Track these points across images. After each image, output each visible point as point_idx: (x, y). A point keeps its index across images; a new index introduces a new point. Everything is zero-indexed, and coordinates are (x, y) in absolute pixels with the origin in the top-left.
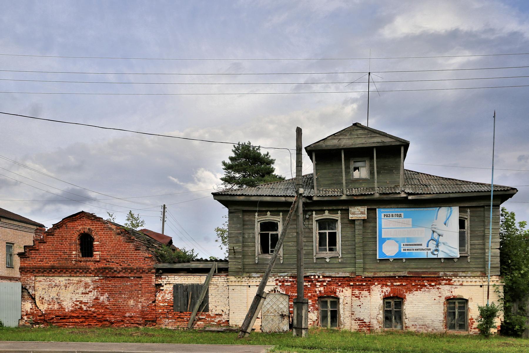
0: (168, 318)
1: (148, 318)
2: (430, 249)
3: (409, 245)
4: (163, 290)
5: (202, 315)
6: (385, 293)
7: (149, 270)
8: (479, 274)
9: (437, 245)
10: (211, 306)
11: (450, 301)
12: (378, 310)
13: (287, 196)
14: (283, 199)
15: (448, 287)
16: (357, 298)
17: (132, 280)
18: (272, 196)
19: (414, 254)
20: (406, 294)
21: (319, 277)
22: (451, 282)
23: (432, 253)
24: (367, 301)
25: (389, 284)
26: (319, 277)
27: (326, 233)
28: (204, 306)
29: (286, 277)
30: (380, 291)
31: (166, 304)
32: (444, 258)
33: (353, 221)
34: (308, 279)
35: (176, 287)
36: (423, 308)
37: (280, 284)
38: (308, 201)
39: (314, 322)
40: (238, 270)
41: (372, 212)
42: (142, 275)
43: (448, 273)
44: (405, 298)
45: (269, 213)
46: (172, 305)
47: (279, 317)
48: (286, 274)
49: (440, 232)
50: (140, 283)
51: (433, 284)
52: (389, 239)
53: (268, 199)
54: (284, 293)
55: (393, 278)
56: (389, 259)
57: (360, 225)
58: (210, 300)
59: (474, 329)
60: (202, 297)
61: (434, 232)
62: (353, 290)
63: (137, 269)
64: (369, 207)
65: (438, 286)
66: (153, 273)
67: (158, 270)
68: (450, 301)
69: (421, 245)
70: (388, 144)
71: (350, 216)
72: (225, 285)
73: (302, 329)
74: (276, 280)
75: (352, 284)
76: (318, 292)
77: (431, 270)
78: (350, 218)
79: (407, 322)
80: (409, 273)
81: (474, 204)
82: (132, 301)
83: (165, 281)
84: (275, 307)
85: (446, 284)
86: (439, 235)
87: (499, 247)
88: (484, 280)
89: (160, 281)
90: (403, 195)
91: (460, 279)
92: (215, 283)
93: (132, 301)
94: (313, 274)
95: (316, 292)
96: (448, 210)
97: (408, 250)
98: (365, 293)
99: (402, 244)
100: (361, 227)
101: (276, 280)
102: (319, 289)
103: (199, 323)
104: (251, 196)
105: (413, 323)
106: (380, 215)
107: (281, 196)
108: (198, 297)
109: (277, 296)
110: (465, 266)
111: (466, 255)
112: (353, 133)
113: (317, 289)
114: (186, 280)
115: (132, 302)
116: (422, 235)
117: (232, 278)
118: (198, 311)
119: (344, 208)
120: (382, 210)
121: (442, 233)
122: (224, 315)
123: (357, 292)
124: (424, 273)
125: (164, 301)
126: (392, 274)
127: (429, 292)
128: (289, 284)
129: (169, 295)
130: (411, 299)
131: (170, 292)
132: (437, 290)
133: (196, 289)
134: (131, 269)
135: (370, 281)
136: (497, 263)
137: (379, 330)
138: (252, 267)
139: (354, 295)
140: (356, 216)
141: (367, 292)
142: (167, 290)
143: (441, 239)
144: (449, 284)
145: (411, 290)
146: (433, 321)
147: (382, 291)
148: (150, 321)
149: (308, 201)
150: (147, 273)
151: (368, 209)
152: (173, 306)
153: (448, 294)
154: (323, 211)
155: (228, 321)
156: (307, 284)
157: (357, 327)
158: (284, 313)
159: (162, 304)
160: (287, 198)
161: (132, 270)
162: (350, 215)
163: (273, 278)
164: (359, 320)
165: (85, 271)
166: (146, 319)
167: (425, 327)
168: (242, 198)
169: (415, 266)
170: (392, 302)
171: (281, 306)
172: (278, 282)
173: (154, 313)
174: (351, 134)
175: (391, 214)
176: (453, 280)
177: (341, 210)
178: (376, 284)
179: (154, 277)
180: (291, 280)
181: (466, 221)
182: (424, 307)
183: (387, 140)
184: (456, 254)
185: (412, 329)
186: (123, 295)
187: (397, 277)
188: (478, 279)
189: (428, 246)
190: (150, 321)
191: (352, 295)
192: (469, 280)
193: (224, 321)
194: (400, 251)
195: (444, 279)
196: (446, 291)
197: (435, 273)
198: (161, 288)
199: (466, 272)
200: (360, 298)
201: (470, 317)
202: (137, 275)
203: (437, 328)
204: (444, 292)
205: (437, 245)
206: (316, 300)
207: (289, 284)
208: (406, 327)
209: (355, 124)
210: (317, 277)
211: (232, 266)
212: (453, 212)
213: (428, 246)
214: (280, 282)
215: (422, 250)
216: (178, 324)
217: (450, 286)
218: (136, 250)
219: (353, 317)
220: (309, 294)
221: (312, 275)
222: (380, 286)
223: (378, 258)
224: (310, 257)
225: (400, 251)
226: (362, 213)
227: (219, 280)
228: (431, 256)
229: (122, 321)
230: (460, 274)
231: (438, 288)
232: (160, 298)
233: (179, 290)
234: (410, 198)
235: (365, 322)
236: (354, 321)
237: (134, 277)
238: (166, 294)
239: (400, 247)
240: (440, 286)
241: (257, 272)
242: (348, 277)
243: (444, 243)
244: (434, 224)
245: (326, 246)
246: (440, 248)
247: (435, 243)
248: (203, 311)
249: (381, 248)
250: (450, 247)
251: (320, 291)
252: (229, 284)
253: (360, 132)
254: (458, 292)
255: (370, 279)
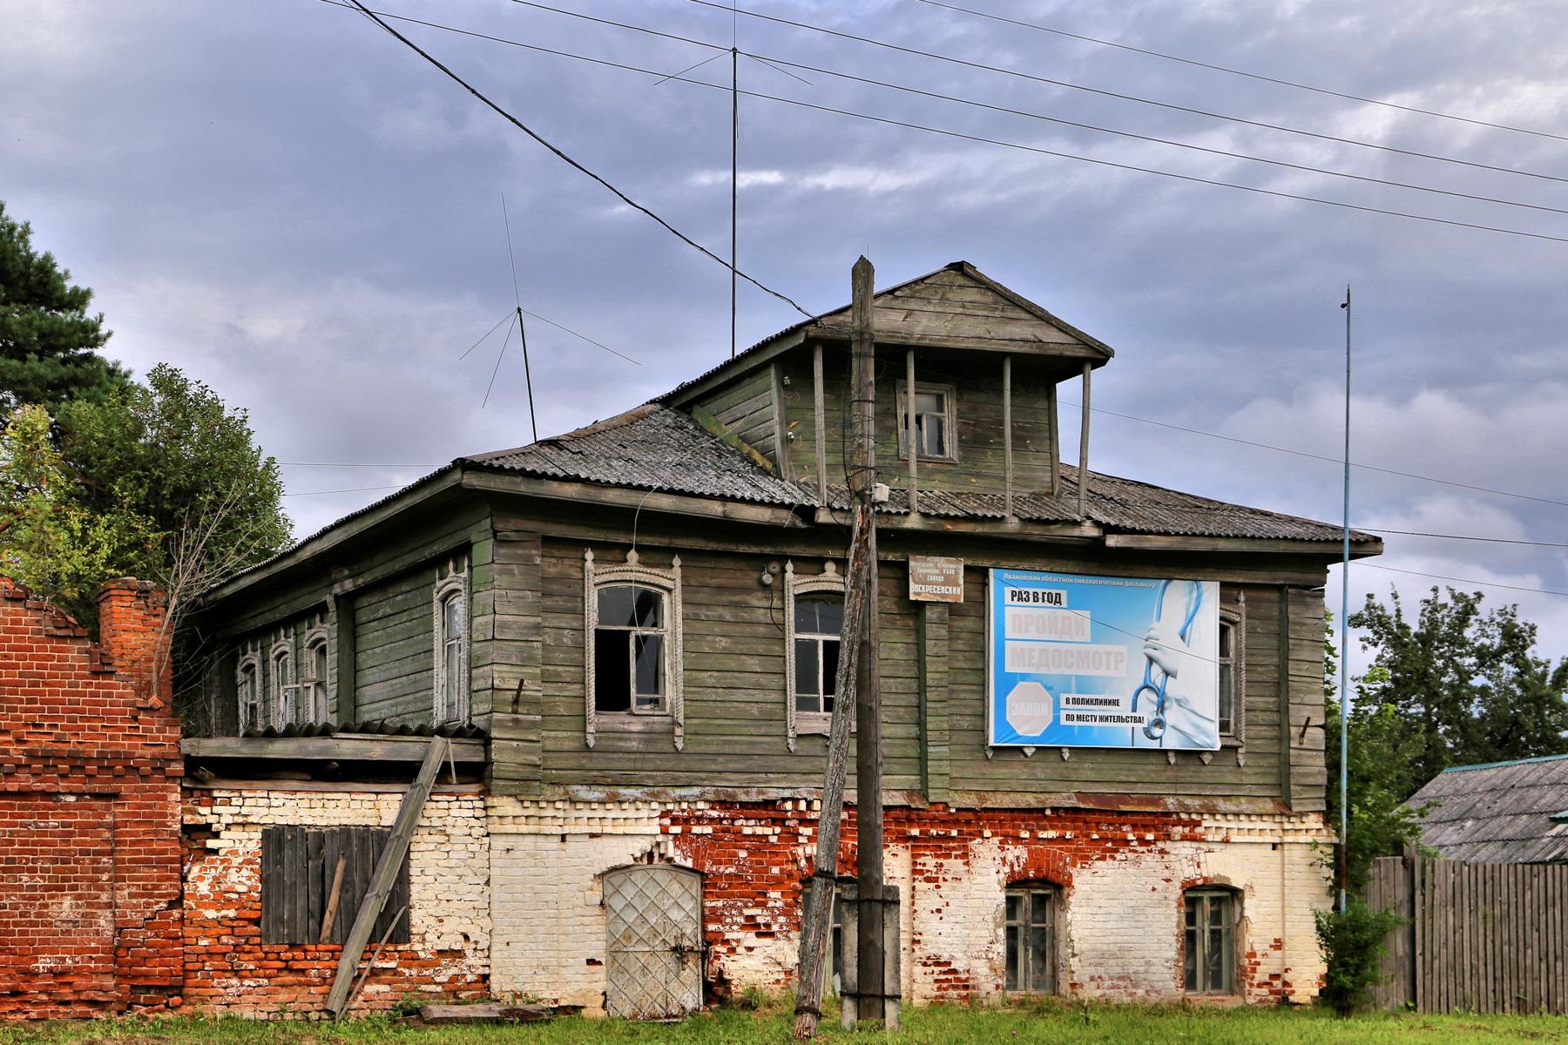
0: (237, 973)
1: (146, 976)
2: (1140, 720)
3: (1088, 702)
4: (215, 852)
5: (384, 955)
6: (1012, 865)
7: (159, 767)
8: (1269, 806)
9: (1161, 708)
10: (419, 919)
11: (1193, 894)
12: (992, 926)
13: (733, 499)
14: (716, 509)
15: (1187, 848)
16: (932, 885)
17: (68, 806)
18: (681, 493)
19: (1096, 733)
20: (1073, 871)
21: (809, 804)
22: (1198, 830)
23: (1147, 732)
24: (960, 895)
25: (1025, 834)
26: (809, 804)
27: (815, 643)
28: (394, 924)
29: (701, 805)
30: (998, 861)
31: (232, 913)
32: (1177, 752)
33: (920, 605)
34: (772, 814)
35: (276, 839)
36: (1122, 919)
37: (677, 829)
38: (799, 524)
39: (789, 973)
40: (526, 772)
41: (978, 577)
42: (124, 788)
43: (1188, 801)
44: (1069, 884)
45: (633, 555)
46: (254, 915)
47: (670, 959)
48: (696, 791)
49: (1169, 666)
50: (109, 819)
51: (1150, 836)
52: (1025, 677)
53: (665, 503)
54: (689, 863)
55: (1034, 815)
56: (1020, 749)
57: (941, 622)
58: (415, 891)
59: (1259, 986)
60: (384, 880)
61: (1151, 660)
62: (914, 856)
63: (102, 756)
64: (969, 563)
65: (1160, 845)
66: (172, 778)
67: (192, 763)
68: (1193, 894)
69: (1115, 703)
70: (1054, 351)
71: (914, 588)
72: (477, 832)
73: (883, 997)
74: (663, 815)
75: (915, 832)
76: (803, 863)
77: (1139, 789)
78: (912, 598)
79: (1078, 968)
80: (1081, 796)
81: (1260, 577)
82: (67, 902)
83: (226, 814)
84: (653, 920)
85: (1184, 838)
86: (1167, 674)
87: (1322, 722)
88: (1287, 826)
89: (205, 815)
90: (1089, 531)
91: (1224, 824)
92: (436, 822)
93: (67, 902)
94: (787, 793)
95: (795, 861)
96: (1191, 592)
97: (1079, 718)
98: (954, 865)
99: (1063, 697)
100: (944, 632)
101: (663, 815)
102: (809, 850)
103: (370, 989)
104: (608, 485)
105: (1092, 971)
106: (1000, 596)
107: (711, 497)
108: (367, 882)
109: (659, 876)
110: (1230, 778)
111: (1236, 743)
112: (950, 296)
113: (800, 850)
114: (319, 811)
115: (66, 907)
116: (1120, 671)
117: (505, 806)
118: (370, 942)
119: (890, 558)
120: (1007, 575)
121: (1166, 662)
122: (469, 953)
123: (929, 862)
124: (1124, 801)
125: (221, 899)
126: (1030, 800)
127: (1137, 863)
128: (708, 830)
129: (245, 872)
130: (1086, 888)
131: (250, 862)
132: (1158, 856)
133: (367, 845)
134: (73, 756)
135: (968, 822)
136: (1320, 773)
137: (996, 997)
138: (572, 763)
139: (921, 872)
140: (929, 588)
141: (960, 861)
142: (234, 853)
143: (1173, 688)
144: (1193, 839)
145: (1088, 858)
146: (1148, 963)
147: (1004, 860)
148: (148, 988)
149: (799, 524)
150: (145, 777)
151: (966, 567)
152: (257, 922)
153: (1190, 872)
154: (817, 565)
155: (485, 977)
156: (768, 831)
157: (930, 990)
158: (686, 943)
159: (211, 914)
160: (730, 506)
161: (77, 762)
162: (911, 584)
163: (655, 805)
164: (937, 964)
165: (611, 776)
166: (141, 982)
167: (1127, 983)
168: (570, 491)
169: (1092, 776)
170: (1025, 897)
171: (676, 915)
172: (667, 821)
173: (175, 955)
174: (944, 299)
175: (1031, 591)
176: (1205, 824)
177: (684, 553)
178: (987, 833)
179: (175, 797)
180: (714, 814)
181: (666, 598)
182: (1119, 912)
183: (1052, 336)
184: (1212, 739)
185: (1089, 993)
186: (25, 877)
187: (1048, 812)
188: (1267, 824)
189: (1134, 710)
190: (148, 988)
191: (914, 872)
192: (1246, 824)
193: (470, 978)
194: (1057, 719)
195: (1180, 822)
196: (1185, 861)
197: (1154, 799)
198: (211, 844)
199: (1234, 801)
200: (941, 883)
201: (1248, 949)
202: (97, 787)
203: (1159, 985)
204: (1177, 866)
205: (1161, 708)
206: (795, 890)
207: (708, 830)
208: (1073, 985)
209: (959, 267)
210: (803, 806)
211: (505, 755)
212: (1204, 597)
213: (1134, 710)
214: (675, 821)
215: (1120, 719)
216: (283, 996)
217: (1195, 845)
218: (96, 674)
219: (918, 953)
220: (775, 870)
221: (785, 800)
222: (996, 840)
223: (992, 743)
224: (774, 731)
225: (1057, 719)
226: (949, 581)
227: (454, 812)
228: (1144, 743)
229: (15, 993)
230: (1222, 805)
231: (1162, 852)
232: (203, 888)
233: (287, 853)
234: (1112, 541)
235: (954, 971)
236: (919, 969)
237: (80, 795)
238: (231, 870)
239: (1057, 708)
240: (1168, 846)
241: (591, 784)
242: (902, 807)
243: (1178, 701)
244: (1152, 633)
245: (817, 692)
246: (1170, 716)
247: (1154, 698)
248: (390, 941)
249: (1001, 706)
250: (1196, 719)
251: (809, 859)
252: (491, 829)
253: (972, 295)
254: (1220, 865)
255: (970, 816)
